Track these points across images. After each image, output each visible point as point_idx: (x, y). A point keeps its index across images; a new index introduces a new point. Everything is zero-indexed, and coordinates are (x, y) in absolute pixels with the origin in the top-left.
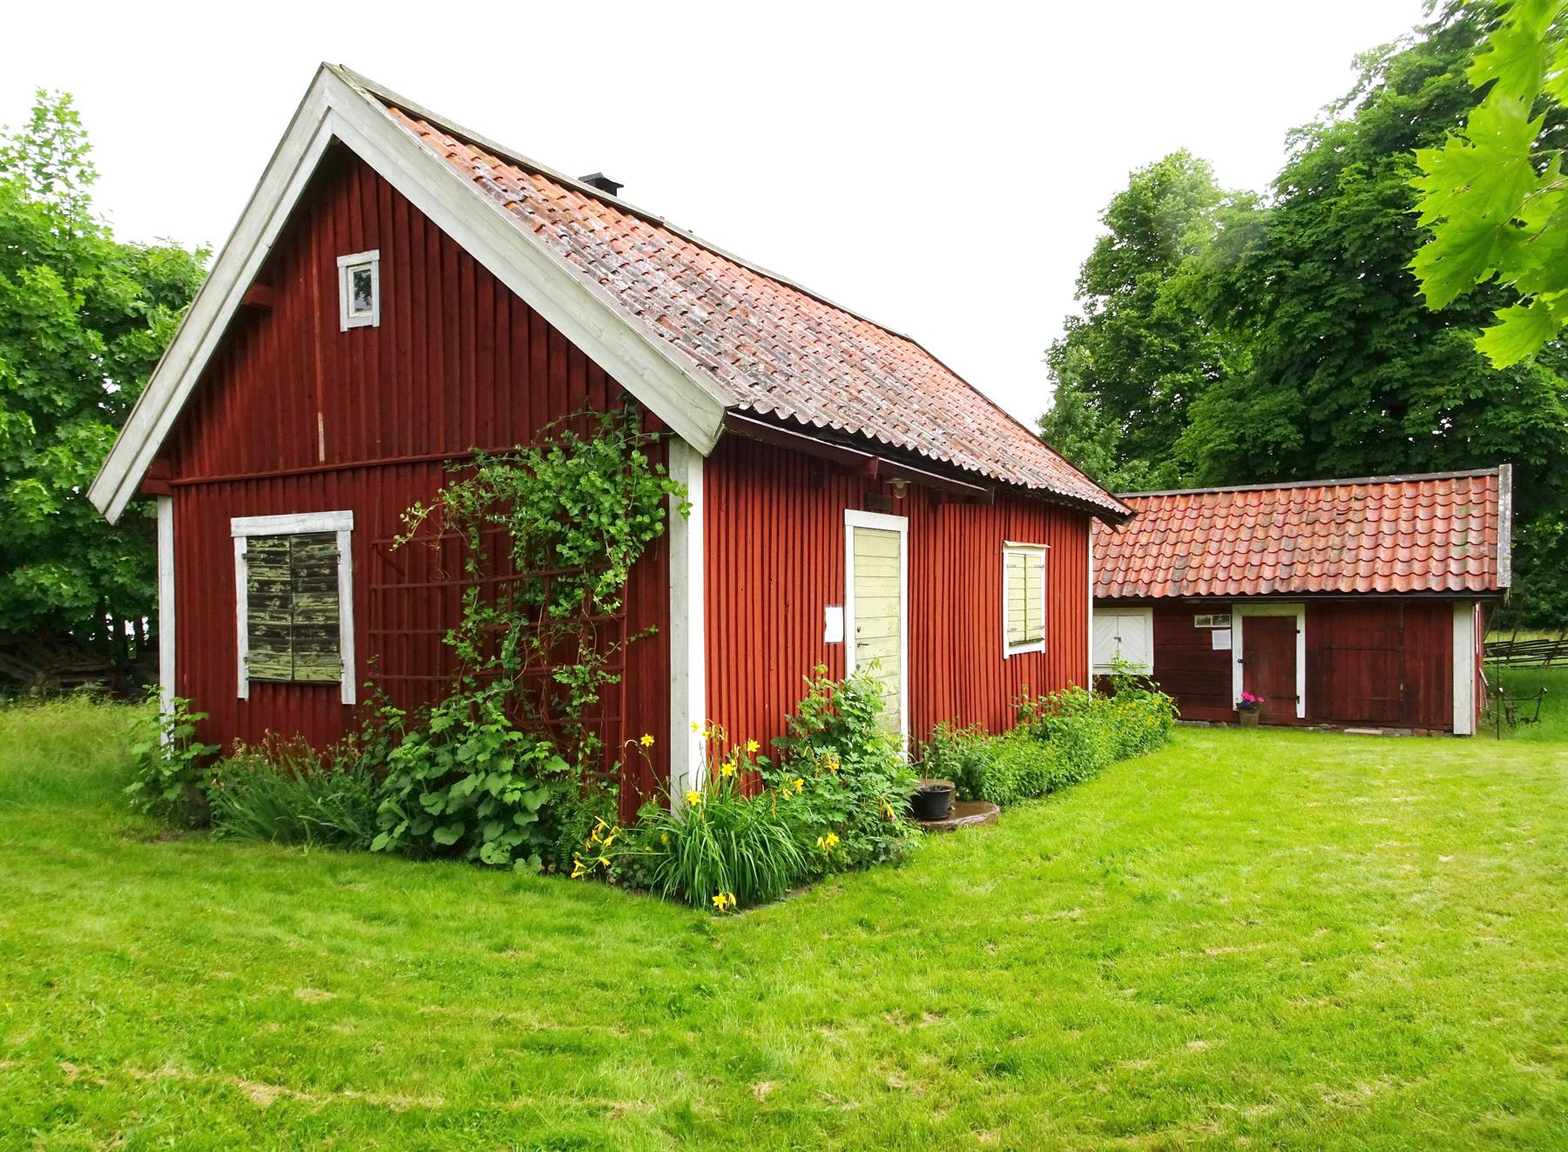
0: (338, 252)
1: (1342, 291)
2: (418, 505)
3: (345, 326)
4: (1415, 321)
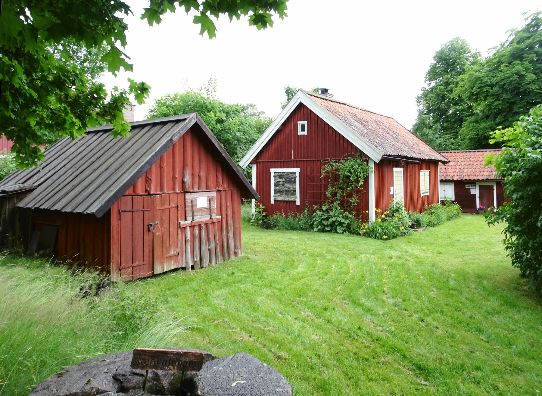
1: (504, 96)
3: (299, 134)
4: (525, 104)
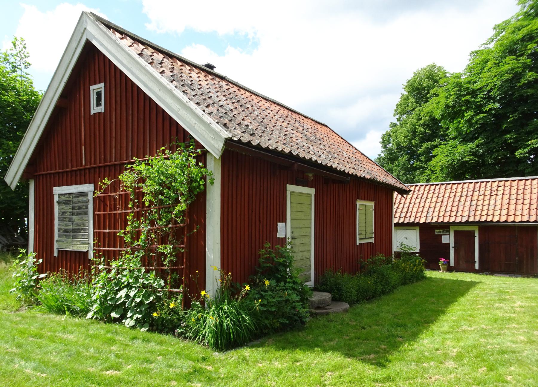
0: (90, 85)
2: (106, 179)
